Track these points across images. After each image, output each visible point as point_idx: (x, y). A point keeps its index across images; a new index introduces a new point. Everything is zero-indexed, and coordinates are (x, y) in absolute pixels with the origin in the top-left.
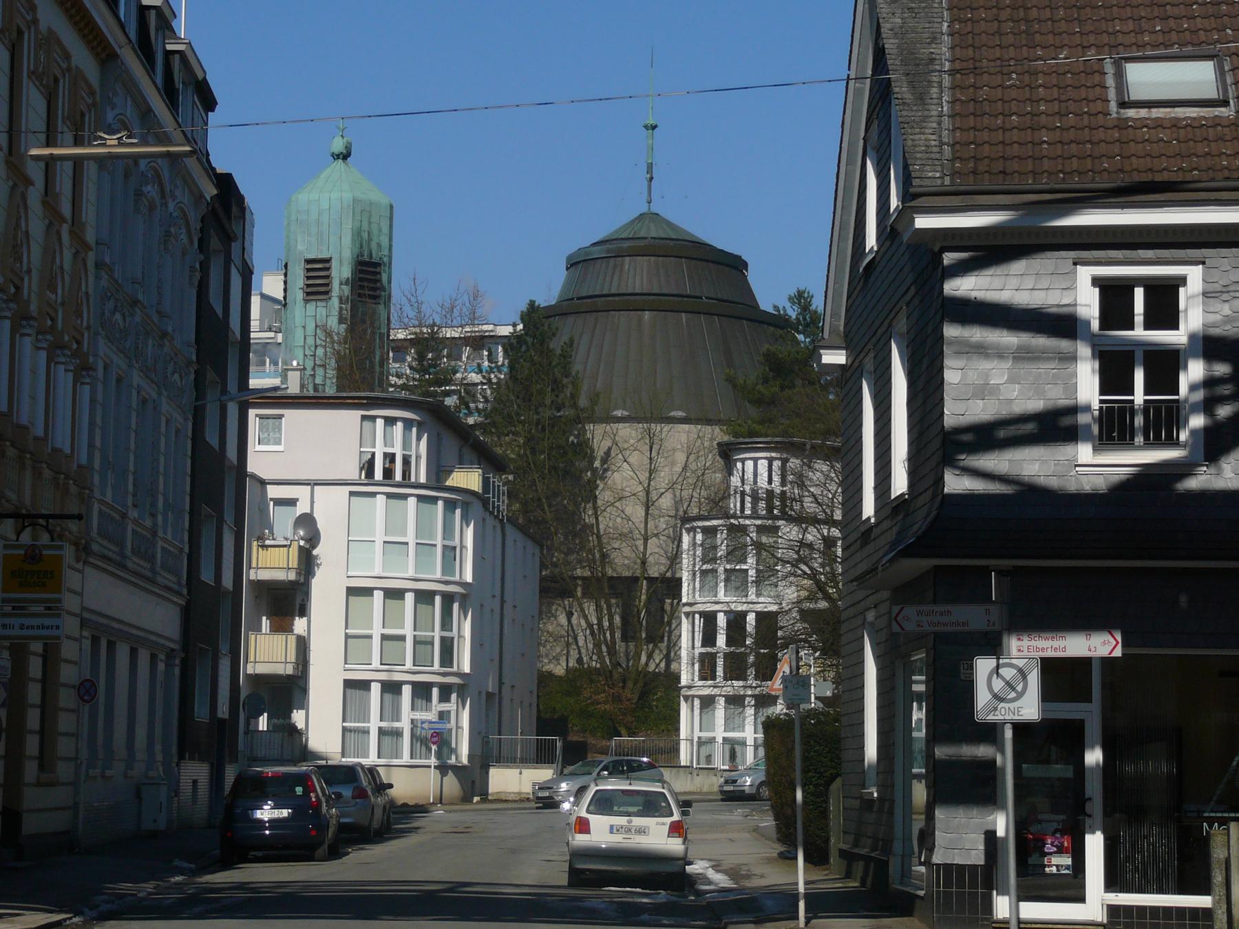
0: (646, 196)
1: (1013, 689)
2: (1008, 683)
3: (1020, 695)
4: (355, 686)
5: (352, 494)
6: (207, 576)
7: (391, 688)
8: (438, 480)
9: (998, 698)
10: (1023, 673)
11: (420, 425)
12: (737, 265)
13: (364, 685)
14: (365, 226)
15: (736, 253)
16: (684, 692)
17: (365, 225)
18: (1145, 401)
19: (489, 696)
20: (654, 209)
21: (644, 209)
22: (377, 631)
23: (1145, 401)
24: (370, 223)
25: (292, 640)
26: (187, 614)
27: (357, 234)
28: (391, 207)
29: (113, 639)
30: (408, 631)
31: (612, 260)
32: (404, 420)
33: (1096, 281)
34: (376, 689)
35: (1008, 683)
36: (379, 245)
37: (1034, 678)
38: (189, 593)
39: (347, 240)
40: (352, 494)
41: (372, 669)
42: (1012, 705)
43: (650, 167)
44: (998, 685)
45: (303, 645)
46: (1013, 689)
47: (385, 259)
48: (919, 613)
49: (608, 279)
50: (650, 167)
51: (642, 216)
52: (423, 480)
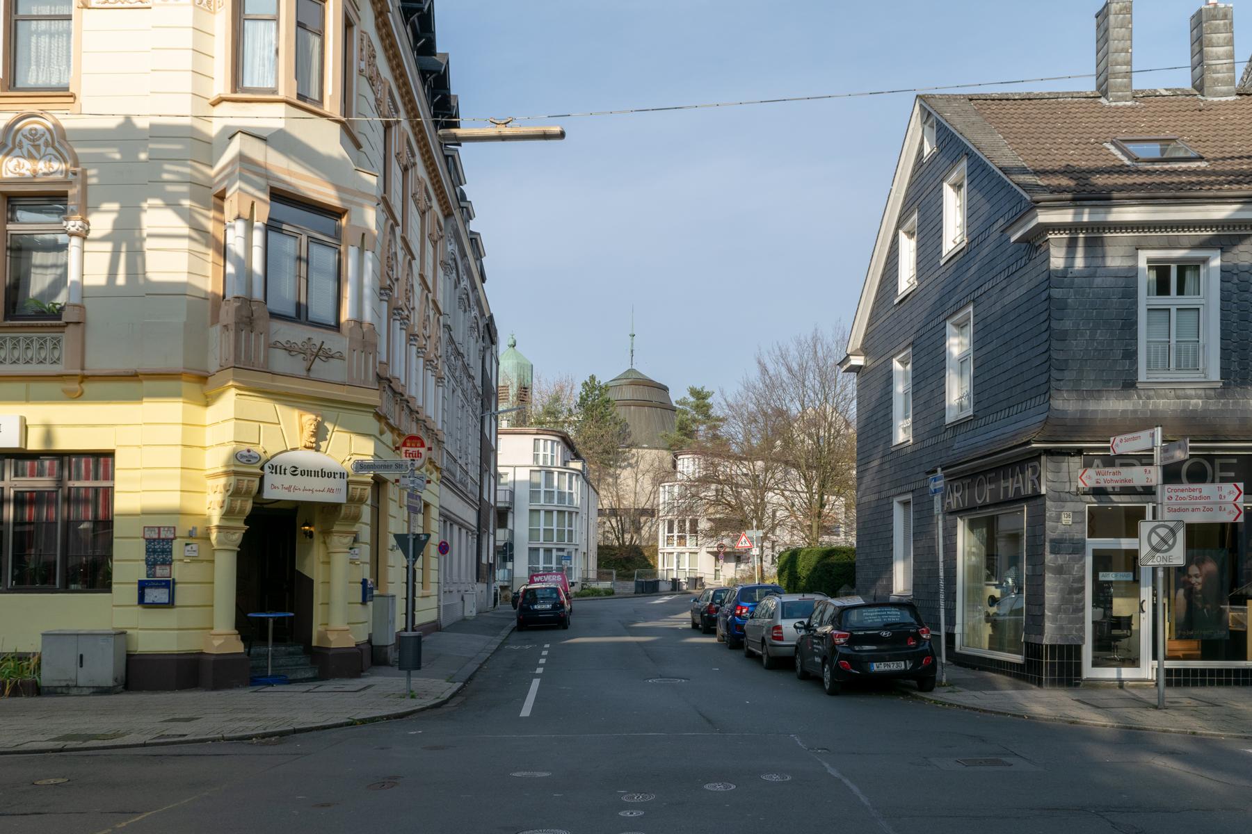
1: (1166, 543)
2: (1162, 539)
3: (1171, 547)
4: (533, 551)
7: (548, 551)
9: (1155, 549)
10: (1173, 532)
12: (665, 389)
13: (537, 549)
22: (542, 527)
27: (519, 376)
33: (953, 324)
34: (542, 551)
35: (1162, 539)
37: (1181, 535)
39: (515, 380)
42: (1165, 555)
44: (1155, 540)
46: (1166, 543)
48: (1098, 473)
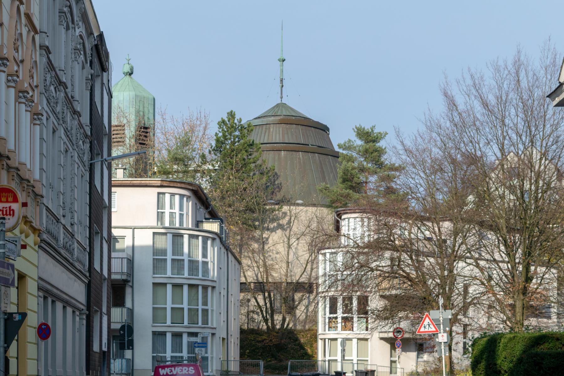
0: (279, 95)
4: (158, 336)
5: (154, 234)
6: (97, 266)
7: (177, 336)
8: (197, 226)
11: (188, 197)
12: (324, 129)
13: (164, 334)
14: (141, 109)
15: (324, 123)
16: (320, 337)
17: (141, 109)
18: (188, 357)
19: (223, 339)
20: (284, 102)
21: (279, 102)
22: (169, 305)
23: (188, 357)
24: (144, 107)
25: (125, 310)
26: (89, 287)
27: (138, 112)
28: (154, 99)
29: (54, 299)
30: (185, 305)
31: (264, 127)
32: (180, 195)
36: (148, 118)
38: (90, 276)
39: (132, 117)
40: (154, 234)
41: (168, 325)
43: (282, 80)
45: (131, 312)
47: (152, 126)
49: (263, 135)
50: (282, 80)
51: (278, 105)
52: (190, 226)
